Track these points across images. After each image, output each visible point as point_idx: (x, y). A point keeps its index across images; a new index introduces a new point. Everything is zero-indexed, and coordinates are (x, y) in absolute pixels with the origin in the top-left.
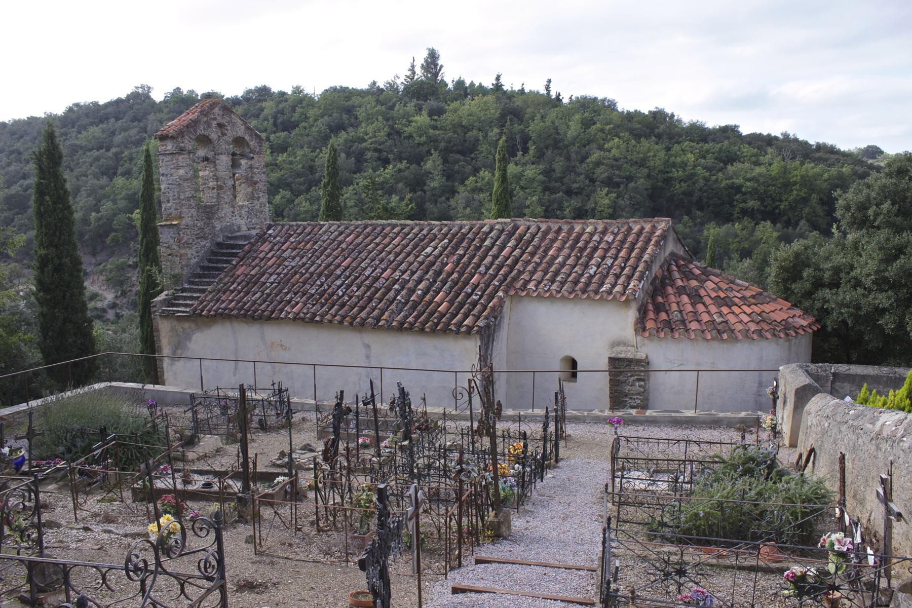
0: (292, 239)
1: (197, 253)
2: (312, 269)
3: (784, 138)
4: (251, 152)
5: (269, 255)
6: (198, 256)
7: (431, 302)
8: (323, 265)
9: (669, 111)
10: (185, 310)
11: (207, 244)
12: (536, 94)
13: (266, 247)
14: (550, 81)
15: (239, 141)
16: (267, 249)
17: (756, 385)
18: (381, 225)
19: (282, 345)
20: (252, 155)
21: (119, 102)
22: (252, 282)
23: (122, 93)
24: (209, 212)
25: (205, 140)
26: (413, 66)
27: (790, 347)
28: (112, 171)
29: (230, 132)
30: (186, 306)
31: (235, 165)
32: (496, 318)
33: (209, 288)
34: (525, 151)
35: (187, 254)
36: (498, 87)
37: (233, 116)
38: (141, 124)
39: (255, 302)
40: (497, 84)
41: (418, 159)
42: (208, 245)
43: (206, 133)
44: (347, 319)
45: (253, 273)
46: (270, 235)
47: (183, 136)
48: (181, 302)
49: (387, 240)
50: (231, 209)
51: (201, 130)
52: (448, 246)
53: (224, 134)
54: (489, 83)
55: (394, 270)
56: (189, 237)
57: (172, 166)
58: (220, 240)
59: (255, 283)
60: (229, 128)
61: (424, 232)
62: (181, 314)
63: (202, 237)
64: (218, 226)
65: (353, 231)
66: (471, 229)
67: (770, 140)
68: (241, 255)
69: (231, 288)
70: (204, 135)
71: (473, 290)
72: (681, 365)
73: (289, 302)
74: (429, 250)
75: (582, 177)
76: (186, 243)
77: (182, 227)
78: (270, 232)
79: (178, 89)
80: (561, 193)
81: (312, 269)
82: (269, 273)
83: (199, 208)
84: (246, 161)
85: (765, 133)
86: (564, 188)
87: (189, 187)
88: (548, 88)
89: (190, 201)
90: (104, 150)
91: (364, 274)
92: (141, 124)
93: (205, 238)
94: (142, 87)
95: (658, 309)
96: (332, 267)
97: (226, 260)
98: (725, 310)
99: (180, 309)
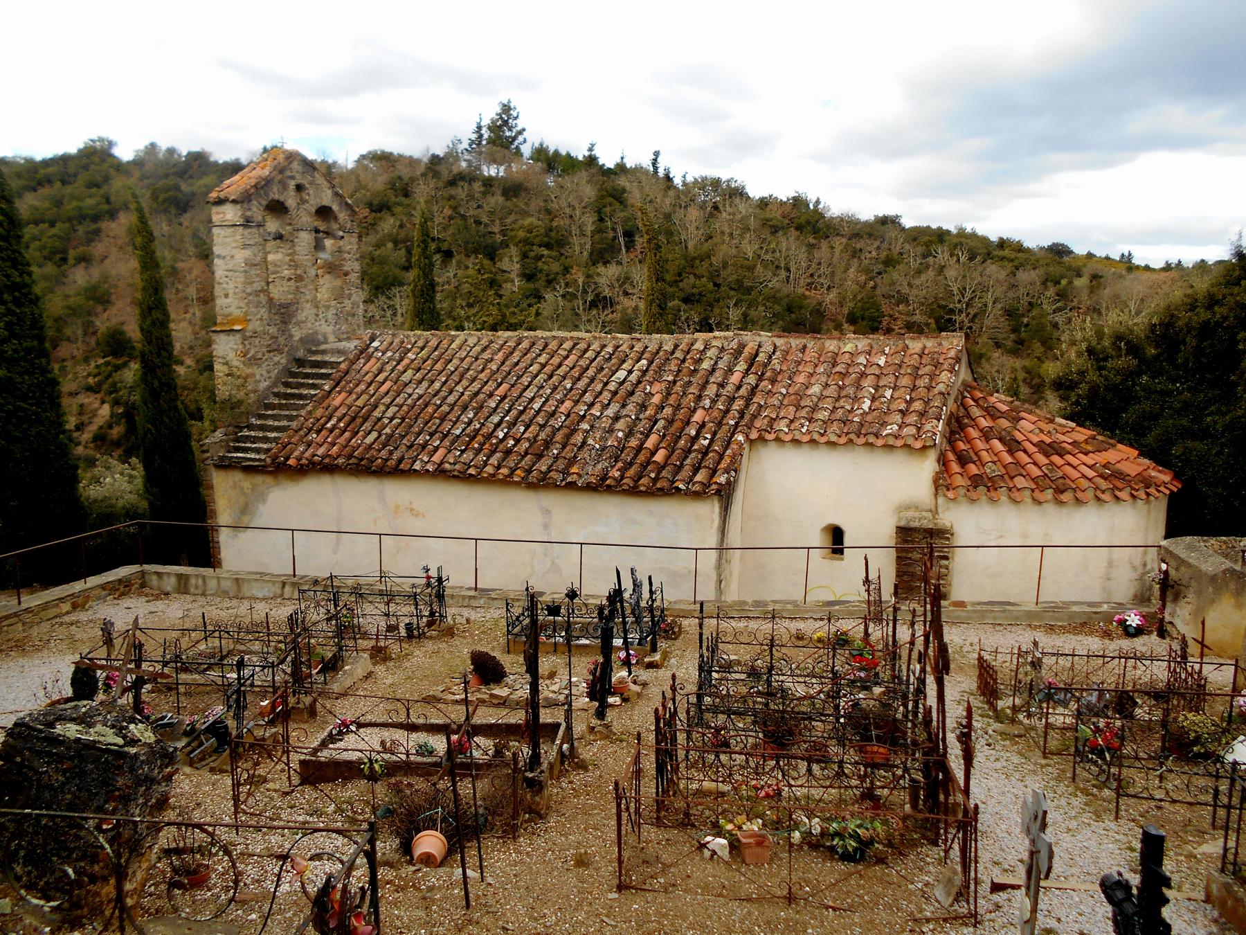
0: (411, 355)
1: (268, 372)
2: (451, 399)
3: (959, 233)
4: (340, 229)
5: (380, 378)
6: (270, 378)
7: (640, 448)
8: (467, 393)
9: (812, 197)
10: (257, 457)
11: (282, 360)
12: (638, 170)
13: (372, 366)
14: (657, 154)
15: (324, 212)
16: (375, 369)
17: (1105, 564)
18: (542, 338)
19: (412, 510)
20: (341, 233)
21: (64, 159)
22: (356, 420)
23: (72, 146)
24: (284, 313)
25: (277, 208)
26: (479, 127)
27: (1149, 511)
28: (59, 256)
29: (312, 197)
30: (257, 451)
31: (318, 246)
32: (736, 471)
33: (294, 424)
34: (630, 245)
35: (253, 375)
36: (591, 160)
37: (316, 174)
38: (102, 192)
39: (370, 447)
40: (590, 156)
41: (492, 253)
42: (284, 361)
43: (282, 199)
44: (519, 472)
45: (360, 403)
46: (376, 349)
47: (250, 201)
48: (249, 445)
49: (556, 360)
50: (314, 311)
51: (275, 194)
52: (647, 370)
53: (303, 201)
54: (580, 154)
55: (576, 402)
56: (257, 349)
57: (234, 245)
58: (301, 354)
59: (365, 419)
60: (311, 192)
61: (610, 349)
62: (251, 463)
63: (275, 350)
64: (297, 334)
65: (502, 346)
66: (676, 346)
67: (941, 236)
68: (337, 376)
69: (329, 425)
70: (278, 201)
71: (698, 433)
72: (1001, 537)
73: (424, 446)
74: (621, 374)
75: (704, 280)
76: (253, 357)
77: (248, 334)
78: (375, 344)
79: (153, 146)
80: (677, 302)
81: (451, 399)
82: (384, 404)
83: (270, 308)
84: (332, 241)
85: (934, 226)
86: (682, 294)
87: (258, 275)
88: (655, 162)
89: (258, 296)
90: (46, 225)
91: (532, 408)
92: (102, 192)
93: (279, 351)
94: (101, 140)
95: (963, 460)
96: (481, 396)
97: (313, 384)
98: (1056, 459)
99: (249, 456)
